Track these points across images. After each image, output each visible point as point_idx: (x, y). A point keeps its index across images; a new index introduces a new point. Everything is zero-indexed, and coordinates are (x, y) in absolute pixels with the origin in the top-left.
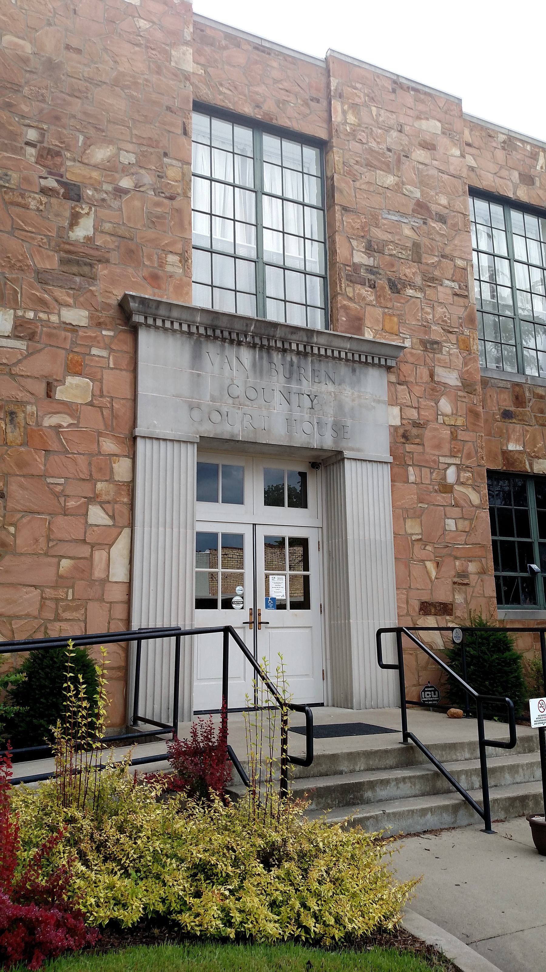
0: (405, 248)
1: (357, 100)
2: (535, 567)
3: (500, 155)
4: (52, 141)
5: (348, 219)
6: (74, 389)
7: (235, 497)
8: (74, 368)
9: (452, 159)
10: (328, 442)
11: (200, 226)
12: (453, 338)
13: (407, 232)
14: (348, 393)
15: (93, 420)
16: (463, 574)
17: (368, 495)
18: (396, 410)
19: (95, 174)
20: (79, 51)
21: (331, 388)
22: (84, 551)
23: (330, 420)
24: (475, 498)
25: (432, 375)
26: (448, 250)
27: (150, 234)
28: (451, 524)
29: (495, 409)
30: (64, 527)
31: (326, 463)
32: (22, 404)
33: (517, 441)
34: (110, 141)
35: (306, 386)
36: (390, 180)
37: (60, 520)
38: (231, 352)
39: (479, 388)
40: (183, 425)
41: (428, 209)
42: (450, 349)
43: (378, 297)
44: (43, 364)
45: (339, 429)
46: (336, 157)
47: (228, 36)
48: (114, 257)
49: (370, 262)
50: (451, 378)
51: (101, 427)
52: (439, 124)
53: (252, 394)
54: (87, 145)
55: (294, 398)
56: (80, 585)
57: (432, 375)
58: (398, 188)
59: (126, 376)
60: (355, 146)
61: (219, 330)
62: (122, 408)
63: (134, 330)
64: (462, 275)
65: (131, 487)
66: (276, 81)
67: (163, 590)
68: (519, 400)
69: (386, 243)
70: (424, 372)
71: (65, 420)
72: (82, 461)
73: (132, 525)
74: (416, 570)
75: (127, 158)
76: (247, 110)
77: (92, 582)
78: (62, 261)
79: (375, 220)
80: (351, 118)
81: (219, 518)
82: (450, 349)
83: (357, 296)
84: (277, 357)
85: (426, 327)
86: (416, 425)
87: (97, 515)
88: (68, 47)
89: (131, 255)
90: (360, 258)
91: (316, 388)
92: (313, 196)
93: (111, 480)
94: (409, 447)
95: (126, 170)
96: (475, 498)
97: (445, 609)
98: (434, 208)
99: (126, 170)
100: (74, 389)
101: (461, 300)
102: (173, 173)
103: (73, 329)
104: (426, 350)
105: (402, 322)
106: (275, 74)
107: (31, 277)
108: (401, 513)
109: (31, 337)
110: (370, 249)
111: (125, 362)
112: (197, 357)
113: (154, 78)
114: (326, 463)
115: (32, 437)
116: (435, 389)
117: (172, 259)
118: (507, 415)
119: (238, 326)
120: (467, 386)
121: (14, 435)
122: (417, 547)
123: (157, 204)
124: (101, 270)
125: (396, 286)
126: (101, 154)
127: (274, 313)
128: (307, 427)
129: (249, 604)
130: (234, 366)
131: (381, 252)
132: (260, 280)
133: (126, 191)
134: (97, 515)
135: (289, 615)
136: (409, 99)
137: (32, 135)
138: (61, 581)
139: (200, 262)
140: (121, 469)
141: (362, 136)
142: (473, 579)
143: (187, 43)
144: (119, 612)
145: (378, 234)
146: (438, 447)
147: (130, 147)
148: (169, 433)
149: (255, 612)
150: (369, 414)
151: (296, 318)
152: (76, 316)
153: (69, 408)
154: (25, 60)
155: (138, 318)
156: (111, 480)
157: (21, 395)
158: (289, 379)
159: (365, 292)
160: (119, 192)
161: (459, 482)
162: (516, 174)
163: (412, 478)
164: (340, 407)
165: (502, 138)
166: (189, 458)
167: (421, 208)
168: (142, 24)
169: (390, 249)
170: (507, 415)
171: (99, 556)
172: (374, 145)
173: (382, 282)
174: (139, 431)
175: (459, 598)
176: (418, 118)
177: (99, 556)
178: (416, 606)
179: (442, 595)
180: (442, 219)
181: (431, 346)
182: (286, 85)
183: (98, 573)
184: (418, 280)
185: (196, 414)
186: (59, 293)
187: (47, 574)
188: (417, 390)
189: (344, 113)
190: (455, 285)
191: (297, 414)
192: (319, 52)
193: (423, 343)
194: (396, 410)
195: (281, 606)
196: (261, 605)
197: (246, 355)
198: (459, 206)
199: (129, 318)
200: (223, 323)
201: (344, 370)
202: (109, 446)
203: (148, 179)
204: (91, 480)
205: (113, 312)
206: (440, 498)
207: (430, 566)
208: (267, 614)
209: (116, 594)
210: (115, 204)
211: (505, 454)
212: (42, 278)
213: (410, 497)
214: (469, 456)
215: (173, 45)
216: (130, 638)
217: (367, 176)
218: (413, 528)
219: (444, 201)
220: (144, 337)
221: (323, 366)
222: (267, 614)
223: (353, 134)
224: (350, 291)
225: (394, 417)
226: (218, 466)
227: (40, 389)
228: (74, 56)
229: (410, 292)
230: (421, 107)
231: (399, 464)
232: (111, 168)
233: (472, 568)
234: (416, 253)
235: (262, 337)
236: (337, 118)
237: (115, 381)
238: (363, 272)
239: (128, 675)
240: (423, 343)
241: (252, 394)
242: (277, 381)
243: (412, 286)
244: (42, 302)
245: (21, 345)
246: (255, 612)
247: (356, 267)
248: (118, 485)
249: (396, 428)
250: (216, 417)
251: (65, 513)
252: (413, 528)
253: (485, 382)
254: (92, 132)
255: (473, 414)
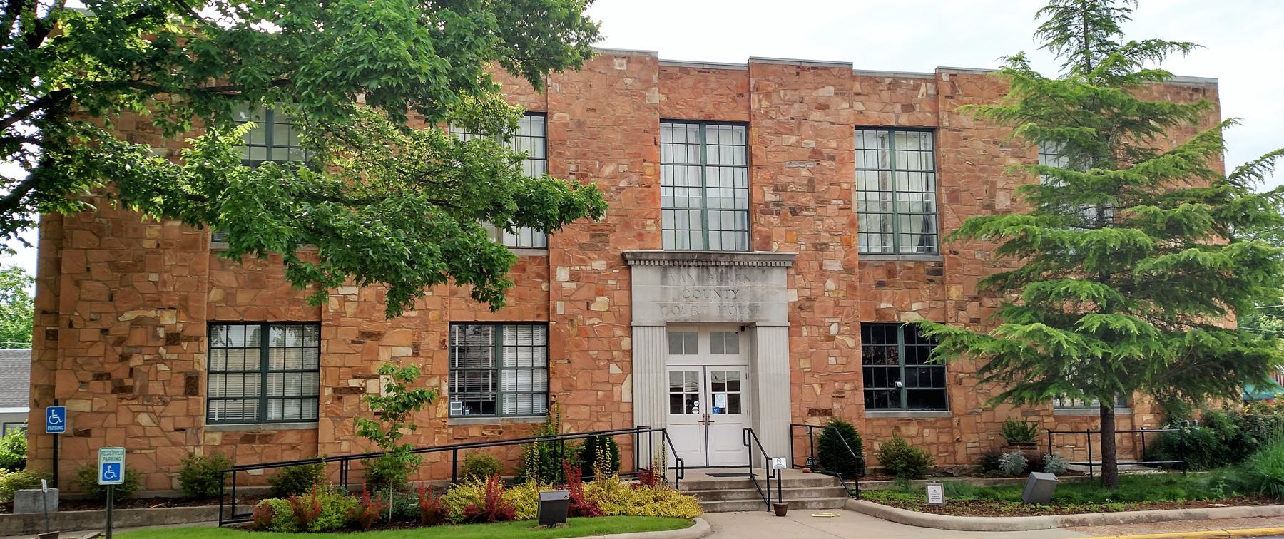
0: (802, 185)
1: (770, 89)
2: (899, 384)
3: (886, 95)
4: (583, 169)
5: (761, 174)
6: (600, 304)
7: (693, 350)
8: (600, 293)
9: (841, 112)
10: (746, 318)
11: (666, 193)
12: (837, 239)
13: (804, 173)
14: (759, 287)
15: (610, 319)
16: (841, 391)
17: (773, 347)
18: (794, 292)
19: (606, 183)
20: (594, 110)
21: (748, 284)
22: (609, 387)
23: (747, 304)
24: (851, 343)
25: (821, 266)
26: (835, 179)
27: (637, 211)
28: (832, 361)
29: (871, 281)
30: (599, 375)
31: (747, 328)
32: (575, 315)
33: (888, 301)
34: (613, 161)
35: (731, 285)
36: (792, 139)
37: (597, 372)
38: (684, 271)
39: (857, 270)
40: (658, 317)
41: (821, 153)
42: (836, 247)
43: (782, 221)
44: (585, 293)
45: (753, 309)
46: (754, 133)
47: (681, 69)
48: (618, 228)
49: (777, 198)
50: (836, 266)
51: (614, 322)
52: (832, 88)
53: (697, 294)
54: (601, 167)
55: (724, 294)
56: (608, 404)
57: (821, 266)
58: (798, 144)
59: (626, 293)
60: (767, 122)
61: (678, 260)
62: (624, 310)
63: (630, 267)
64: (846, 196)
65: (630, 353)
66: (713, 90)
67: (650, 405)
68: (891, 273)
69: (789, 184)
70: (815, 264)
71: (596, 321)
72: (605, 341)
73: (632, 373)
74: (807, 390)
75: (623, 168)
76: (695, 116)
77: (614, 402)
78: (592, 236)
79: (780, 170)
80: (765, 104)
81: (683, 363)
82: (836, 247)
83: (767, 223)
84: (712, 270)
85: (818, 235)
86: (808, 299)
87: (614, 369)
88: (588, 110)
89: (627, 225)
90: (770, 197)
91: (738, 286)
92: (740, 158)
93: (620, 350)
94: (803, 314)
95: (623, 176)
96: (851, 343)
97: (826, 412)
98: (825, 151)
99: (623, 176)
100: (600, 304)
101: (845, 212)
102: (649, 170)
103: (598, 272)
104: (817, 249)
105: (799, 233)
106: (713, 85)
107: (576, 248)
108: (794, 355)
109: (578, 280)
110: (776, 190)
111: (625, 285)
112: (664, 277)
113: (636, 114)
114: (747, 328)
115: (582, 332)
116: (823, 274)
117: (650, 222)
118: (880, 284)
119: (688, 257)
120: (848, 270)
121: (573, 331)
122: (807, 376)
123: (641, 192)
124: (612, 237)
125: (794, 212)
126: (608, 170)
127: (714, 246)
128: (732, 310)
129: (702, 410)
130: (687, 280)
131: (785, 190)
132: (704, 221)
133: (623, 189)
134: (614, 369)
135: (727, 417)
136: (809, 76)
137: (572, 168)
138: (599, 402)
139: (667, 220)
140: (625, 343)
141: (772, 114)
142: (847, 394)
143: (655, 85)
144: (628, 417)
145: (783, 179)
146: (825, 312)
147: (624, 161)
148: (649, 322)
149: (706, 416)
150: (775, 296)
151: (729, 246)
152: (600, 265)
153: (598, 314)
154: (566, 125)
155: (631, 262)
156: (620, 350)
157: (575, 311)
158: (720, 282)
159: (774, 219)
160: (620, 189)
161: (839, 333)
162: (899, 106)
163: (805, 334)
164: (754, 295)
165: (887, 81)
166: (661, 334)
167: (816, 153)
168: (629, 81)
169: (792, 187)
170: (880, 284)
171: (616, 389)
172: (781, 118)
173: (785, 210)
174: (633, 323)
175: (836, 406)
176: (816, 88)
177: (616, 389)
178: (806, 411)
179: (824, 405)
180: (832, 158)
181: (821, 247)
182: (720, 91)
183: (616, 398)
184: (812, 204)
185: (664, 310)
186: (591, 254)
187: (592, 399)
188: (809, 277)
189: (760, 101)
190: (841, 202)
191: (725, 303)
192: (743, 60)
193: (815, 246)
194: (794, 292)
195: (722, 411)
196: (710, 411)
197: (693, 272)
198: (846, 145)
199: (626, 262)
200: (679, 257)
201: (756, 272)
202: (618, 332)
203: (635, 178)
204: (611, 351)
205: (618, 259)
206: (825, 345)
207: (817, 387)
208: (714, 417)
209: (626, 408)
210: (617, 197)
211: (878, 311)
212: (582, 247)
213: (803, 344)
214: (847, 316)
215: (647, 89)
216: (634, 432)
217: (775, 140)
218: (805, 364)
219: (833, 144)
220: (634, 270)
221: (743, 271)
222: (713, 417)
223: (766, 115)
224: (762, 221)
225: (793, 296)
226: (681, 335)
227: (584, 306)
228: (591, 114)
229: (806, 213)
230: (819, 80)
231: (794, 325)
232: (615, 176)
233: (847, 387)
234: (811, 185)
235: (704, 261)
236: (754, 106)
237: (620, 296)
238: (771, 206)
239: (634, 448)
240: (815, 246)
241: (697, 294)
242: (713, 284)
243: (808, 209)
244: (583, 260)
245: (573, 285)
246: (706, 416)
247: (767, 204)
248: (624, 352)
249: (794, 303)
250: (676, 310)
251: (599, 368)
252: (805, 364)
253: (862, 265)
254: (603, 158)
255: (852, 287)
